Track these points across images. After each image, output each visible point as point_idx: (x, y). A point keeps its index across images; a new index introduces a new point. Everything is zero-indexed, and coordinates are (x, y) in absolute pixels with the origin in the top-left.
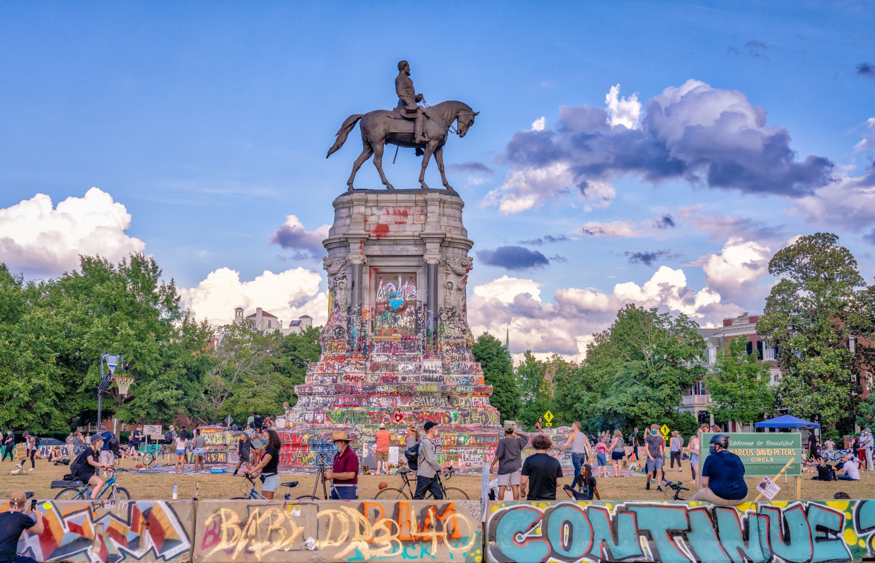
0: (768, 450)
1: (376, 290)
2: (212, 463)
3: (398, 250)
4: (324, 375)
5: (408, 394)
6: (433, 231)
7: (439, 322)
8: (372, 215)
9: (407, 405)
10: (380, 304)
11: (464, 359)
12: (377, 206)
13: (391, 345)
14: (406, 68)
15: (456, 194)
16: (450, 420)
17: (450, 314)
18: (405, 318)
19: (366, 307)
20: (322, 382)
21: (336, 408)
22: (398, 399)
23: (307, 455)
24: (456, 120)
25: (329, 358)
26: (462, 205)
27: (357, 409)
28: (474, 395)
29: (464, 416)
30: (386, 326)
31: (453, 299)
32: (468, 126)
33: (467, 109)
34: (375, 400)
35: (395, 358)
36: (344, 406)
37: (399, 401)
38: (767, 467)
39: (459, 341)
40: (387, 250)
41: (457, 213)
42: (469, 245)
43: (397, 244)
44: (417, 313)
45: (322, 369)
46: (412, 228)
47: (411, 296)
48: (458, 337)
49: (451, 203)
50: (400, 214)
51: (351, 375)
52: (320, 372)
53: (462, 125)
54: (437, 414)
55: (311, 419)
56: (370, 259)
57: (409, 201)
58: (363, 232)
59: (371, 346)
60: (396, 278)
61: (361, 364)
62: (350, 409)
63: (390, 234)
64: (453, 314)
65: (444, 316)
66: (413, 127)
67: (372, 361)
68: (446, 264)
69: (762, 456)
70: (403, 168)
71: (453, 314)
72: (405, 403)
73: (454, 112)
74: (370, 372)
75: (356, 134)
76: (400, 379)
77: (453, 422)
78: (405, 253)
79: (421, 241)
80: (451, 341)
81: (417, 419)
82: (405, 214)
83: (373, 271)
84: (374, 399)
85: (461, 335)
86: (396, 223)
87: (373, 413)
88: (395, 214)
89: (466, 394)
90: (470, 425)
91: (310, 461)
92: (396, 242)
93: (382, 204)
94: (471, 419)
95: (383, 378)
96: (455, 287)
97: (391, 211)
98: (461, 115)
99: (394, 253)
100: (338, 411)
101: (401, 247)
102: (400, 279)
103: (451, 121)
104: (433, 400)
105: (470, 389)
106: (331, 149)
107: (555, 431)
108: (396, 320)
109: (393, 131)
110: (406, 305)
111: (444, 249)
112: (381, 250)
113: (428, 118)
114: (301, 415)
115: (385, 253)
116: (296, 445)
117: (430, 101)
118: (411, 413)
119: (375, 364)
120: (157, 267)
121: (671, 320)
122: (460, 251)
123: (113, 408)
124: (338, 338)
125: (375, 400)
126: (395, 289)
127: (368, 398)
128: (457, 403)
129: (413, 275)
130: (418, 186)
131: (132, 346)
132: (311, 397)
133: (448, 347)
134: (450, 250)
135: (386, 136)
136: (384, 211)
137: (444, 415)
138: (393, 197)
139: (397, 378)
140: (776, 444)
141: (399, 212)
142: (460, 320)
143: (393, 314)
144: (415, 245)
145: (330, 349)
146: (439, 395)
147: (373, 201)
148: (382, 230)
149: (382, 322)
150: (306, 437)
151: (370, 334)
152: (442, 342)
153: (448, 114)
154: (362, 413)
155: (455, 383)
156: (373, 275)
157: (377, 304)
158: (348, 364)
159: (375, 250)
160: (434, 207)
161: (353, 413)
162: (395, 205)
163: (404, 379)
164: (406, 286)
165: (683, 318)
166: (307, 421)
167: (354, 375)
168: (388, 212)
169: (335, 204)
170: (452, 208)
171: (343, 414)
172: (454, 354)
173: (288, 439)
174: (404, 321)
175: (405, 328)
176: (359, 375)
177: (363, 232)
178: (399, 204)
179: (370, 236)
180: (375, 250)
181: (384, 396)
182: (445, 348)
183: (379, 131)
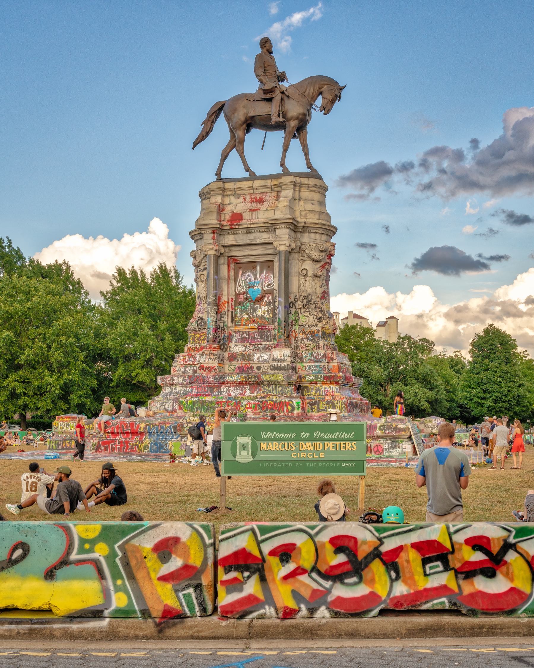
1: (236, 279)
2: (66, 449)
3: (251, 238)
4: (186, 365)
5: (256, 384)
6: (282, 216)
7: (293, 311)
8: (230, 204)
9: (255, 394)
10: (239, 294)
11: (318, 347)
12: (234, 195)
13: (249, 335)
14: (267, 45)
15: (320, 178)
16: (293, 409)
17: (305, 301)
18: (263, 308)
19: (225, 298)
20: (184, 373)
21: (188, 398)
22: (247, 388)
23: (142, 442)
24: (320, 96)
25: (192, 350)
26: (326, 189)
27: (207, 398)
28: (323, 383)
29: (312, 405)
30: (245, 317)
31: (310, 286)
32: (333, 102)
33: (331, 82)
34: (225, 390)
35: (251, 348)
36: (197, 395)
37: (248, 390)
38: (291, 465)
39: (314, 329)
40: (241, 239)
41: (317, 197)
42: (331, 231)
43: (250, 233)
44: (274, 302)
45: (184, 360)
46: (263, 216)
47: (269, 285)
48: (312, 326)
49: (309, 186)
50: (256, 201)
51: (205, 365)
52: (182, 363)
53: (326, 101)
54: (280, 403)
55: (170, 408)
56: (227, 249)
57: (265, 187)
58: (215, 221)
59: (229, 338)
60: (255, 268)
61: (214, 355)
62: (201, 398)
63: (243, 222)
64: (309, 302)
65: (299, 304)
66: (278, 107)
67: (230, 351)
68: (300, 250)
69: (307, 451)
70: (265, 151)
71: (309, 302)
72: (253, 392)
73: (317, 88)
74: (228, 362)
75: (222, 126)
76: (255, 368)
77: (296, 411)
78: (258, 241)
79: (271, 227)
80: (307, 329)
81: (262, 408)
82: (261, 201)
83: (232, 261)
84: (224, 389)
85: (316, 322)
86: (251, 210)
87: (221, 402)
88: (251, 201)
89: (316, 383)
90: (317, 414)
91: (145, 448)
93: (240, 192)
94: (319, 408)
95: (239, 368)
96: (310, 273)
97: (248, 198)
98: (327, 91)
99: (248, 242)
100: (190, 400)
101: (254, 235)
102: (258, 268)
103: (314, 99)
104: (280, 389)
105: (320, 378)
106: (197, 139)
107: (383, 420)
108: (254, 310)
109: (251, 114)
110: (265, 294)
111: (299, 235)
112: (236, 240)
114: (161, 405)
115: (240, 242)
116: (135, 433)
117: (294, 78)
118: (256, 402)
119: (233, 354)
120: (179, 274)
122: (318, 236)
123: (145, 399)
124: (200, 330)
125: (225, 390)
126: (253, 279)
127: (219, 387)
128: (308, 391)
129: (270, 264)
130: (279, 170)
131: (149, 345)
132: (173, 388)
133: (304, 336)
134: (306, 235)
135: (246, 120)
136: (241, 199)
137: (288, 404)
138: (257, 183)
139: (252, 368)
140: (328, 435)
141: (256, 199)
142: (316, 307)
143: (252, 304)
144: (268, 231)
145: (194, 340)
146: (285, 384)
147: (230, 190)
148: (237, 217)
149: (242, 311)
150: (142, 425)
151: (230, 324)
152: (297, 331)
153: (310, 91)
154: (211, 402)
155: (307, 371)
156: (232, 266)
157: (237, 294)
158: (202, 355)
159: (230, 239)
160: (287, 191)
161: (203, 402)
162: (252, 192)
163: (259, 368)
164: (264, 275)
165: (127, 280)
166: (167, 410)
167: (208, 365)
168: (245, 199)
169: (200, 195)
170: (311, 191)
171: (194, 403)
172: (309, 343)
173: (127, 427)
174: (262, 311)
175: (263, 317)
176: (212, 365)
177: (215, 221)
178: (255, 191)
179: (223, 225)
180: (230, 239)
181: (234, 386)
182: (301, 336)
183: (240, 116)
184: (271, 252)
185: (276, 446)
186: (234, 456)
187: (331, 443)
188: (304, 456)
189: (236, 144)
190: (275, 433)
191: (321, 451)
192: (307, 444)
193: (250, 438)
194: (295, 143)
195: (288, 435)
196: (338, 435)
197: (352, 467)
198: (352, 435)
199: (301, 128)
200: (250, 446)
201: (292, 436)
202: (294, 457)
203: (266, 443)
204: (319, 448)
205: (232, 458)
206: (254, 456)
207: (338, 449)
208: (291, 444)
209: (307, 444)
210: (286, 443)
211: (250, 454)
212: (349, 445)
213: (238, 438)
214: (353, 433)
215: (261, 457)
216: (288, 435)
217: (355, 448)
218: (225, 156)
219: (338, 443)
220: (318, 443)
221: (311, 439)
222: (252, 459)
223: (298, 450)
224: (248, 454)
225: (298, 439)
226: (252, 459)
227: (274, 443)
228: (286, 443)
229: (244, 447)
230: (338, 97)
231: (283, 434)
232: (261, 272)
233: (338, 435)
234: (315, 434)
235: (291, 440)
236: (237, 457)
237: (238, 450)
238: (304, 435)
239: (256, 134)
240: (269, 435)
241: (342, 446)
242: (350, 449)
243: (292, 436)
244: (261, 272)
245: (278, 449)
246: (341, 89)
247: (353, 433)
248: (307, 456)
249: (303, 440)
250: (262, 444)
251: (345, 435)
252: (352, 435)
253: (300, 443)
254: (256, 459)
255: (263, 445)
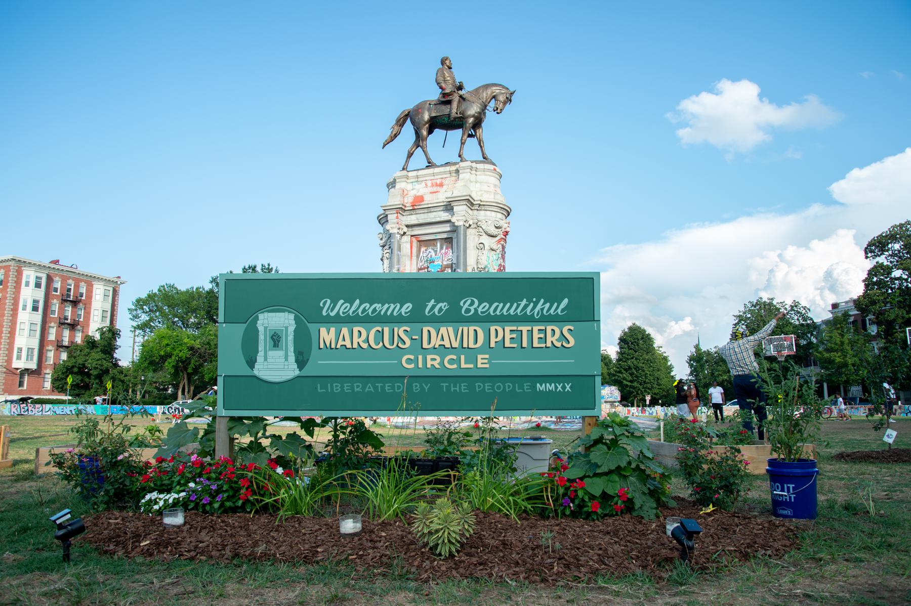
0: (469, 330)
38: (464, 387)
50: (437, 185)
69: (443, 350)
75: (409, 127)
78: (438, 220)
82: (441, 185)
88: (432, 186)
92: (429, 209)
96: (487, 247)
97: (429, 183)
99: (429, 221)
102: (439, 245)
113: (464, 99)
115: (421, 221)
121: (787, 307)
126: (433, 254)
134: (482, 213)
136: (423, 184)
138: (437, 170)
140: (498, 308)
148: (420, 199)
164: (443, 251)
184: (448, 229)
185: (361, 336)
186: (251, 363)
187: (507, 329)
188: (436, 364)
189: (419, 141)
190: (358, 301)
191: (480, 350)
192: (443, 330)
193: (292, 316)
194: (472, 143)
195: (393, 309)
196: (526, 306)
197: (563, 393)
198: (562, 306)
199: (477, 124)
200: (291, 337)
201: (403, 310)
202: (407, 364)
203: (333, 330)
204: (476, 342)
205: (245, 370)
206: (301, 363)
207: (525, 345)
208: (400, 331)
209: (443, 330)
210: (386, 330)
211: (292, 357)
212: (554, 334)
213: (261, 316)
214: (566, 301)
215: (318, 365)
216: (393, 309)
217: (572, 342)
218: (410, 155)
219: (525, 329)
220: (472, 329)
221: (454, 317)
222: (297, 372)
223: (419, 348)
224: (286, 359)
225: (417, 318)
226: (297, 372)
227: (356, 330)
228: (386, 330)
229: (276, 340)
230: (509, 100)
231: (378, 306)
232: (441, 248)
233: (526, 306)
234: (465, 304)
235: (400, 320)
236: (256, 366)
237: (261, 347)
238: (433, 307)
239: (439, 133)
240: (342, 307)
241: (536, 335)
242: (558, 344)
243: (403, 310)
244: (441, 248)
245: (365, 346)
246: (512, 94)
247: (566, 301)
248: (442, 363)
249: (435, 320)
250: (323, 331)
251: (542, 306)
252: (562, 306)
253: (425, 330)
254: (308, 371)
255: (327, 335)
